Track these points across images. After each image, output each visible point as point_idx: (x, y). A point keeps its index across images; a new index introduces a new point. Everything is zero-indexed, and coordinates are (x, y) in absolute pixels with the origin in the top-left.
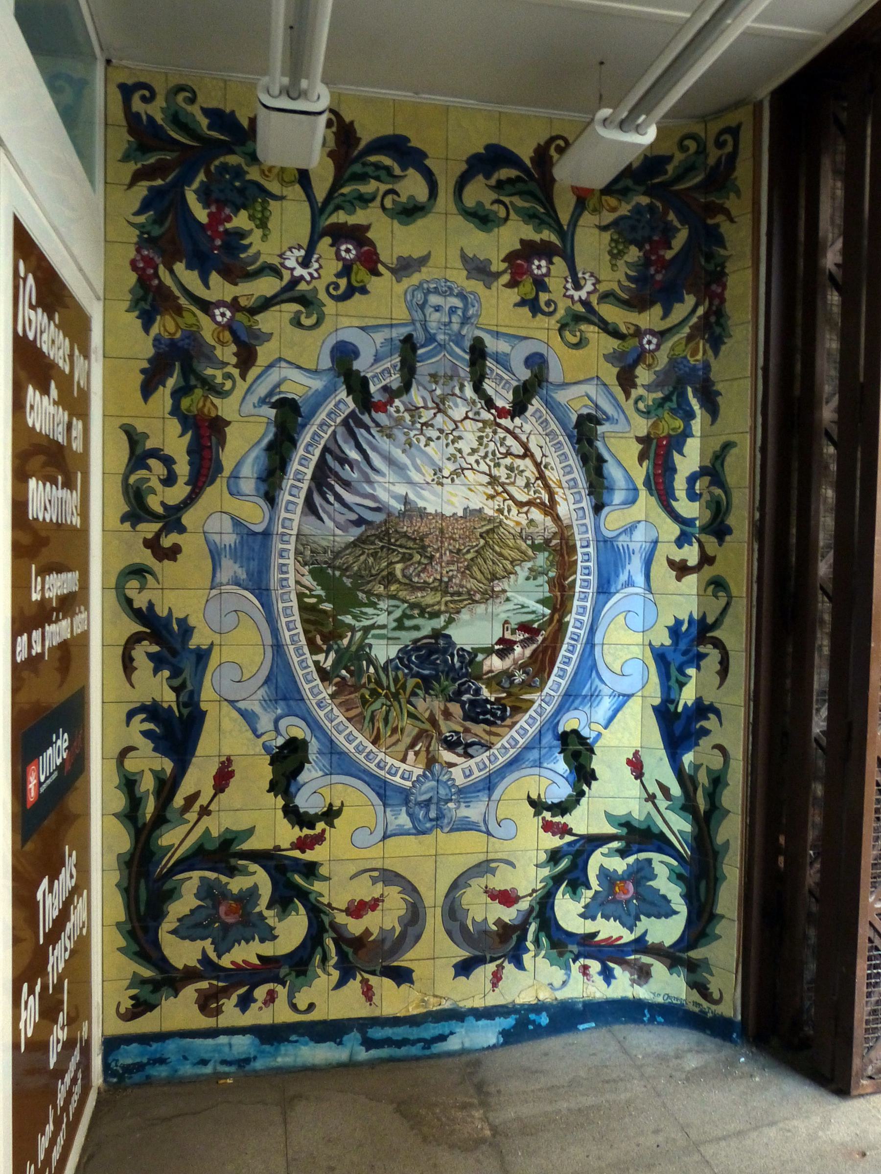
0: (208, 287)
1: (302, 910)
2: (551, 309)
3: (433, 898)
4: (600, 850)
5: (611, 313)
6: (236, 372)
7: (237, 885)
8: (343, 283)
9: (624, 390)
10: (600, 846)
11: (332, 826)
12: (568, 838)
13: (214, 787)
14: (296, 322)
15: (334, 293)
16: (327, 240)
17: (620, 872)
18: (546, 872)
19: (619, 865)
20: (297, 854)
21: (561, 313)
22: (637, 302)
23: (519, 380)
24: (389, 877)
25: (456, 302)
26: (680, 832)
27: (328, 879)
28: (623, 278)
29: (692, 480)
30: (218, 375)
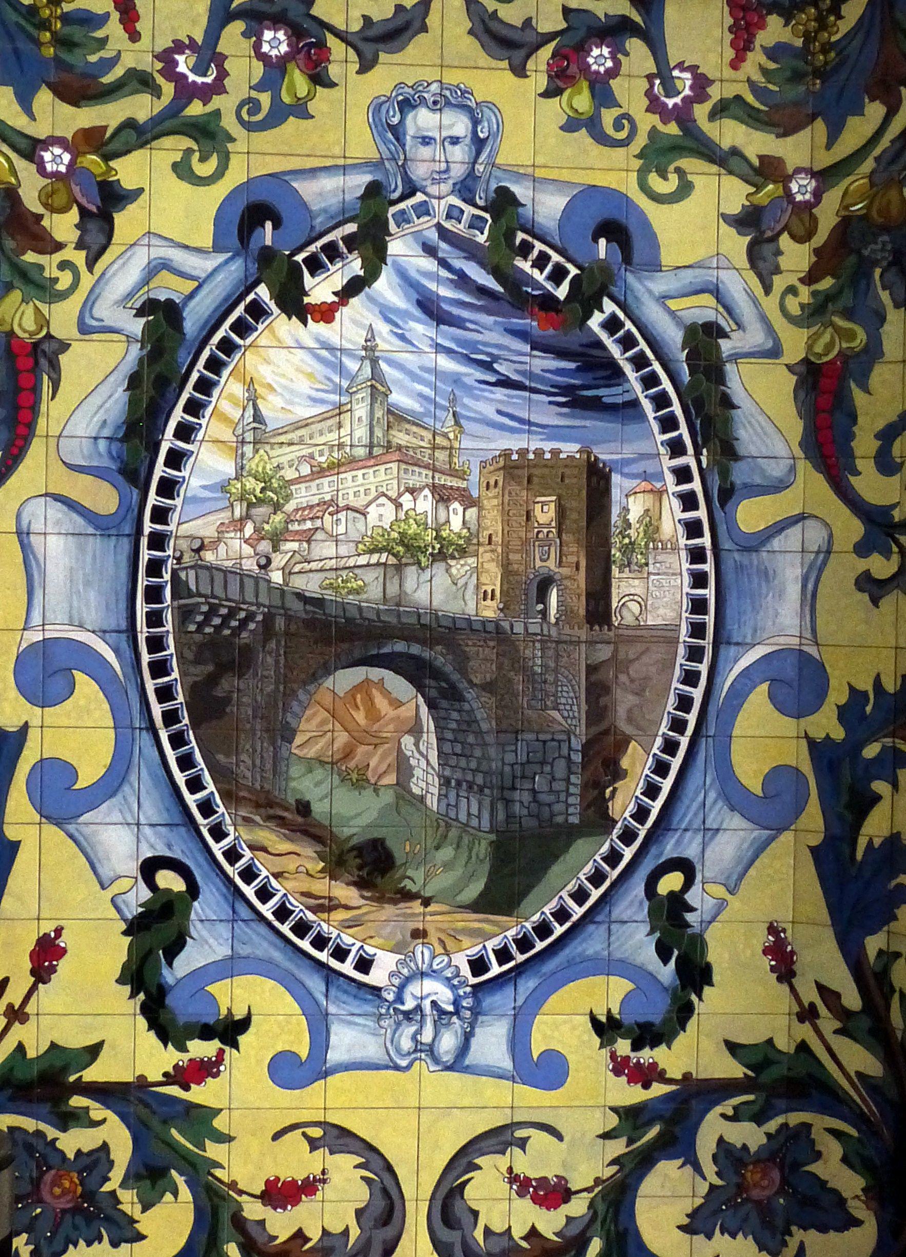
0: (32, 117)
1: (185, 1193)
2: (622, 135)
3: (418, 1190)
4: (719, 1109)
5: (730, 134)
6: (80, 258)
7: (72, 1142)
8: (265, 99)
9: (760, 276)
10: (717, 1103)
11: (235, 1045)
12: (658, 1090)
13: (33, 972)
14: (182, 170)
15: (245, 117)
16: (237, 27)
17: (753, 1148)
18: (618, 1147)
19: (750, 1136)
20: (174, 1091)
21: (641, 140)
22: (781, 121)
23: (735, 357)
24: (338, 1138)
25: (460, 125)
26: (858, 1074)
27: (229, 1139)
28: (757, 77)
29: (887, 436)
30: (50, 263)
